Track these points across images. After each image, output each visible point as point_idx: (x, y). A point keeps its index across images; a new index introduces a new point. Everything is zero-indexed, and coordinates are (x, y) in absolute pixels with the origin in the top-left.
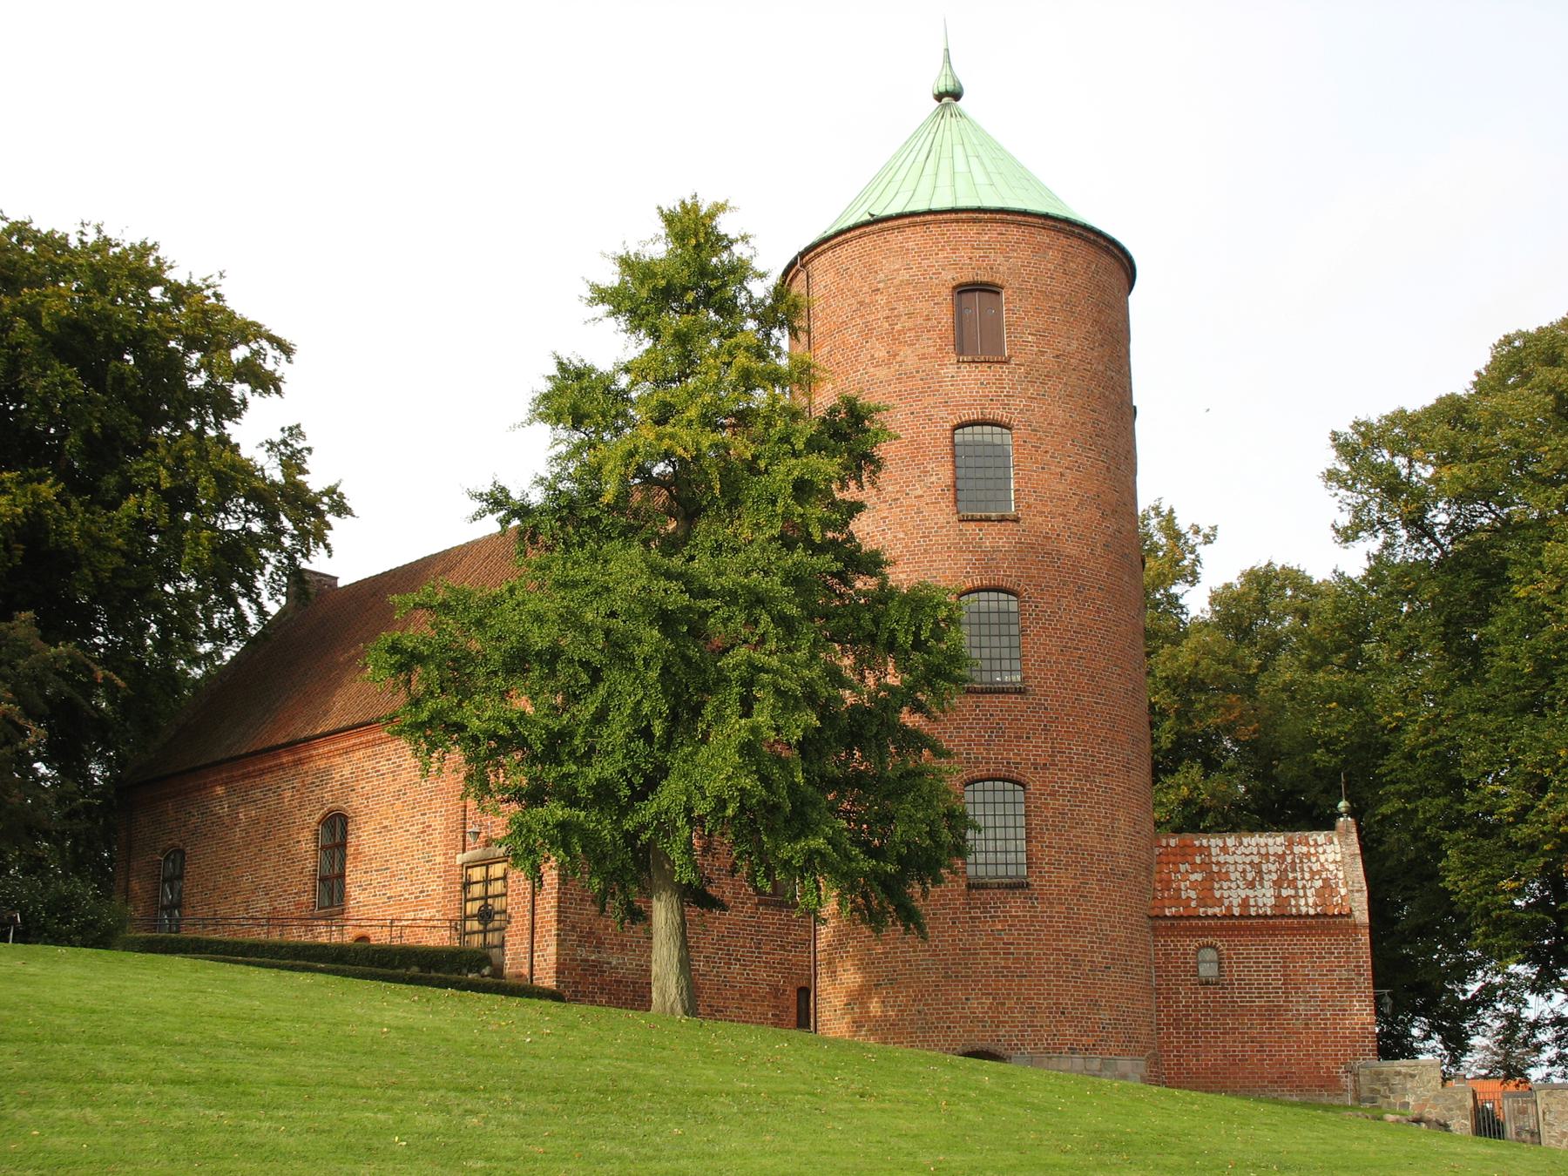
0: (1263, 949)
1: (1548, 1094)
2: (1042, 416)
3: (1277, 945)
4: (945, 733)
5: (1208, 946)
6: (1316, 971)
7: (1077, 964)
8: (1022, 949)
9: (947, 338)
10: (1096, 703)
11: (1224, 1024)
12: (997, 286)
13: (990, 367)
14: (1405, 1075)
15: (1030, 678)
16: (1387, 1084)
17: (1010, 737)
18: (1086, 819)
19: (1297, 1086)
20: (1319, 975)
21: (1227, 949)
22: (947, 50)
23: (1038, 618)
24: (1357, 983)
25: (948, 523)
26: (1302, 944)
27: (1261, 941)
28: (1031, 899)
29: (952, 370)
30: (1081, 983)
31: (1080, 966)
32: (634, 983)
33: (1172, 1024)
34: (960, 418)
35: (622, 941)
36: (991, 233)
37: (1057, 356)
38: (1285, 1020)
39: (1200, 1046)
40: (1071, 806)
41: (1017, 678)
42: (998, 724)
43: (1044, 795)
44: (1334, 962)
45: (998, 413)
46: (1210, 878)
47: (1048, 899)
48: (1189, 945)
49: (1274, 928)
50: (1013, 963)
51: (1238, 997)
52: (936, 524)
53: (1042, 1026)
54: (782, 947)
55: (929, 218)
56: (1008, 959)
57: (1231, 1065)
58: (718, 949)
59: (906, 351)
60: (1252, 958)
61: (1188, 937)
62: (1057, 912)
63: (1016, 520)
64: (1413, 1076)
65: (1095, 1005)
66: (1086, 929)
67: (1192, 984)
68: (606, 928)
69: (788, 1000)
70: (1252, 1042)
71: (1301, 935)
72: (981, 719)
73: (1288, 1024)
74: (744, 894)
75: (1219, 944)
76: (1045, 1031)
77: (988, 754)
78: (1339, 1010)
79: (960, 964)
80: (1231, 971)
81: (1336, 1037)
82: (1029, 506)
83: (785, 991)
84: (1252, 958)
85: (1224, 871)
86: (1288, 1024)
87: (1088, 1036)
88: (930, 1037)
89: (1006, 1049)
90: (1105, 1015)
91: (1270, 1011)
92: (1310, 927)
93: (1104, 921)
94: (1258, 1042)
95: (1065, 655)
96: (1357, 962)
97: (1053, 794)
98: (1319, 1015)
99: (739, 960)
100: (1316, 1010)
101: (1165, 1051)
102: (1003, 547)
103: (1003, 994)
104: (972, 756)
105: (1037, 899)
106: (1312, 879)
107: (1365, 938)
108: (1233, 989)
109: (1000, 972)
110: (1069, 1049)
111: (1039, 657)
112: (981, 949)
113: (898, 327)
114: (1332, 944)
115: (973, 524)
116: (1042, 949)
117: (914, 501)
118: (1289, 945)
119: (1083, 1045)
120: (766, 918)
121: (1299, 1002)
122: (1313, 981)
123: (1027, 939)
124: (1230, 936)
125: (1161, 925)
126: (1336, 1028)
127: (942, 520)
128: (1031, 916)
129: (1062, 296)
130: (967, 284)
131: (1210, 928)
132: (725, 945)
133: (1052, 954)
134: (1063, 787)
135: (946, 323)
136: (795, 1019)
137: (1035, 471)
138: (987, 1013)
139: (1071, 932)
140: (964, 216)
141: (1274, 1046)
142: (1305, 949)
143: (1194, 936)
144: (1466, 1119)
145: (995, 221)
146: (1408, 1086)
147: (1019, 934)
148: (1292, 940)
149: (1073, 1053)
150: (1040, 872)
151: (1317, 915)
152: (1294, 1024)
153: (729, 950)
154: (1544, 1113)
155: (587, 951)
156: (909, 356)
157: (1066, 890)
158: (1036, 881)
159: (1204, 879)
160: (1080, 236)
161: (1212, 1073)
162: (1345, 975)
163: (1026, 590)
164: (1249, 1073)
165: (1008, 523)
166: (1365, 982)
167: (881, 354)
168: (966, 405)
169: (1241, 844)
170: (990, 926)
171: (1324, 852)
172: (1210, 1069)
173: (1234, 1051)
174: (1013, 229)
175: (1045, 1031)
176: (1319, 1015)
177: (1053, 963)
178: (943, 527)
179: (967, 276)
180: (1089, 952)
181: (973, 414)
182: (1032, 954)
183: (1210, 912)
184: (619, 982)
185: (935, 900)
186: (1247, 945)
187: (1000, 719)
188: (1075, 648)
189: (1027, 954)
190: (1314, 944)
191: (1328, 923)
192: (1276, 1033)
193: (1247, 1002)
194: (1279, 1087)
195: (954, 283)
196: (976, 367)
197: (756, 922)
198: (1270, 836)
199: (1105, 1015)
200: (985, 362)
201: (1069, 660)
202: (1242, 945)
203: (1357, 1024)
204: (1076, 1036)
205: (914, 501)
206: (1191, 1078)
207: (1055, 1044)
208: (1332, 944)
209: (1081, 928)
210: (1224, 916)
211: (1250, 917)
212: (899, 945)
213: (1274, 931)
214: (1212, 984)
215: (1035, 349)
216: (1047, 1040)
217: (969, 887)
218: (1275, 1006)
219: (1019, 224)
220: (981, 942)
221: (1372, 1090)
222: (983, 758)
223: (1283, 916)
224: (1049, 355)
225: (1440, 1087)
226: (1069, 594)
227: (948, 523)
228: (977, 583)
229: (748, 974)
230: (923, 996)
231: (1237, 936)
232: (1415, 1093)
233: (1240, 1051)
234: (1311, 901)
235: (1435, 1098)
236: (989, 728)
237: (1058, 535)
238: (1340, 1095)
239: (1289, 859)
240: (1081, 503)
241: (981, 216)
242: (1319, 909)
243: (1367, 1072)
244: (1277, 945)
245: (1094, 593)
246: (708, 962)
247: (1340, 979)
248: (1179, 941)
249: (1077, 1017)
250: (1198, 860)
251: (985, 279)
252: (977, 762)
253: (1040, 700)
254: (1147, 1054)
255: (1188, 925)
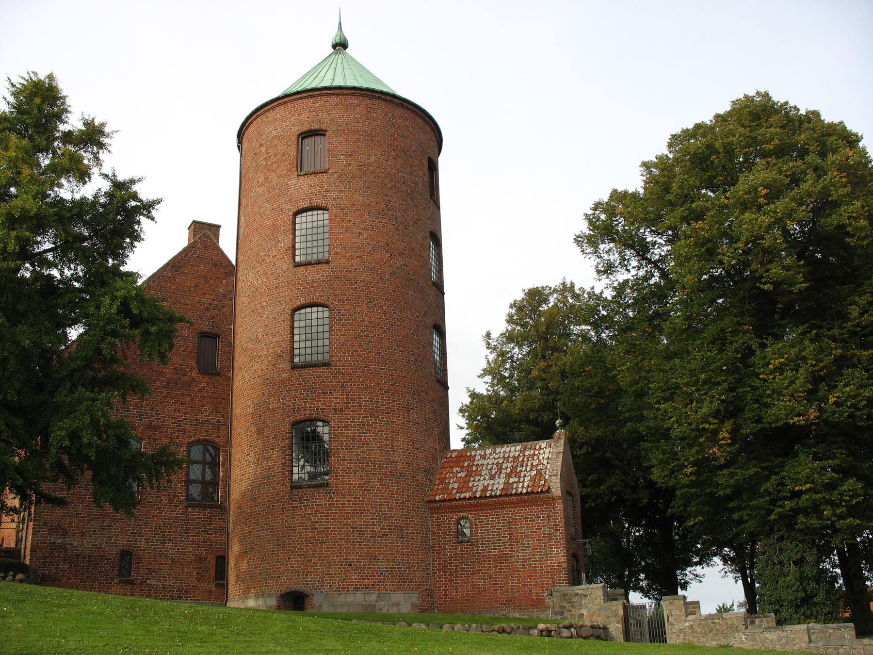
0: (496, 518)
1: (670, 603)
2: (347, 200)
3: (505, 514)
4: (282, 394)
5: (464, 518)
6: (530, 529)
7: (361, 533)
8: (323, 525)
9: (293, 164)
10: (380, 369)
11: (473, 568)
12: (322, 130)
13: (316, 176)
14: (581, 595)
15: (334, 356)
16: (570, 602)
17: (319, 393)
18: (371, 441)
19: (518, 606)
20: (531, 532)
21: (475, 519)
22: (340, 23)
23: (340, 319)
24: (555, 536)
25: (288, 269)
26: (520, 513)
27: (495, 512)
28: (329, 493)
29: (294, 181)
30: (364, 545)
31: (364, 534)
32: (90, 556)
33: (441, 570)
34: (298, 207)
35: (82, 530)
36: (320, 102)
37: (360, 166)
38: (510, 563)
39: (459, 583)
40: (360, 433)
41: (327, 356)
42: (312, 386)
43: (340, 427)
44: (541, 523)
45: (320, 202)
46: (470, 474)
47: (341, 493)
48: (452, 518)
49: (503, 503)
50: (317, 535)
51: (481, 550)
52: (282, 270)
53: (335, 574)
54: (205, 532)
55: (286, 99)
56: (315, 532)
57: (477, 594)
58: (155, 534)
59: (273, 175)
60: (490, 524)
61: (451, 513)
62: (347, 501)
63: (327, 262)
64: (585, 596)
65: (375, 559)
66: (369, 510)
67: (453, 543)
68: (71, 523)
69: (209, 564)
70: (490, 578)
71: (520, 507)
72: (302, 384)
73: (512, 565)
74: (177, 501)
75: (470, 516)
76: (337, 577)
77: (306, 404)
78: (544, 555)
79: (286, 537)
80: (477, 533)
81: (542, 573)
82: (337, 254)
83: (206, 558)
84: (490, 524)
85: (479, 470)
86: (512, 565)
87: (369, 579)
88: (269, 583)
89: (311, 590)
90: (383, 566)
91: (501, 557)
92: (525, 501)
93: (383, 505)
94: (493, 578)
95: (358, 341)
96: (555, 522)
97: (347, 427)
98: (531, 558)
99: (172, 541)
100: (529, 555)
101: (438, 587)
102: (319, 279)
103: (310, 554)
104: (296, 407)
105: (333, 493)
106: (531, 470)
107: (560, 507)
108: (478, 544)
109: (309, 541)
110: (354, 588)
111: (339, 343)
112: (298, 526)
113: (269, 163)
114: (539, 512)
115: (302, 268)
116: (336, 525)
117: (271, 259)
118: (512, 514)
119: (365, 585)
120: (193, 515)
121: (519, 550)
122: (528, 536)
123: (326, 519)
124: (476, 510)
125: (433, 506)
126: (541, 567)
127: (285, 268)
128: (329, 504)
129: (365, 131)
130: (306, 132)
131: (464, 506)
132: (161, 532)
133: (343, 528)
134: (354, 422)
135: (293, 155)
136: (214, 575)
137: (342, 233)
138: (300, 567)
139: (357, 513)
140: (304, 95)
141: (504, 581)
142: (522, 516)
143: (455, 512)
144: (619, 623)
145: (323, 95)
146: (583, 602)
147: (322, 516)
148: (514, 511)
149: (357, 591)
150: (336, 476)
151: (527, 493)
152: (515, 565)
153: (164, 535)
154: (668, 617)
155: (54, 537)
156: (273, 176)
157: (354, 487)
158: (333, 482)
159: (466, 476)
160: (379, 98)
161: (466, 600)
162: (547, 531)
163: (333, 303)
164: (488, 599)
165: (323, 264)
166: (560, 535)
167: (261, 180)
168: (301, 199)
169: (495, 452)
170: (303, 512)
171: (544, 452)
172: (465, 597)
173: (479, 585)
174: (334, 98)
175: (337, 577)
176: (531, 558)
177: (344, 534)
178: (285, 272)
179: (306, 128)
180: (371, 525)
181: (305, 204)
182: (330, 528)
183: (463, 496)
184: (78, 556)
185: (274, 498)
186: (487, 516)
187: (313, 383)
188: (365, 336)
189: (326, 528)
190: (528, 512)
191: (536, 497)
192: (504, 572)
193: (487, 552)
194: (507, 607)
195: (298, 133)
196: (308, 177)
197: (186, 517)
198: (513, 446)
199: (383, 566)
200: (313, 173)
201: (361, 343)
202: (483, 516)
203: (555, 563)
204: (359, 579)
205: (271, 259)
206: (453, 603)
207: (344, 585)
208: (539, 512)
209: (365, 510)
210: (470, 498)
211: (486, 497)
212: (256, 526)
213: (503, 505)
214: (465, 542)
215: (345, 163)
216: (338, 583)
217: (292, 488)
218: (504, 554)
219: (337, 95)
220: (298, 522)
221: (561, 607)
222: (302, 408)
223: (506, 495)
224: (354, 164)
225: (602, 603)
226: (363, 304)
227: (288, 269)
228: (303, 302)
229: (178, 549)
230: (266, 558)
231: (480, 510)
232: (588, 608)
233: (482, 585)
234: (526, 484)
235: (599, 610)
236: (307, 389)
237: (356, 269)
238: (545, 610)
239: (521, 459)
240: (374, 249)
241: (315, 93)
242: (529, 490)
243: (558, 595)
244: (505, 514)
245: (381, 302)
246: (147, 542)
247: (544, 534)
248: (445, 516)
249: (361, 567)
250: (466, 464)
251: (316, 127)
252: (299, 410)
253: (339, 369)
254: (420, 590)
255: (450, 505)
